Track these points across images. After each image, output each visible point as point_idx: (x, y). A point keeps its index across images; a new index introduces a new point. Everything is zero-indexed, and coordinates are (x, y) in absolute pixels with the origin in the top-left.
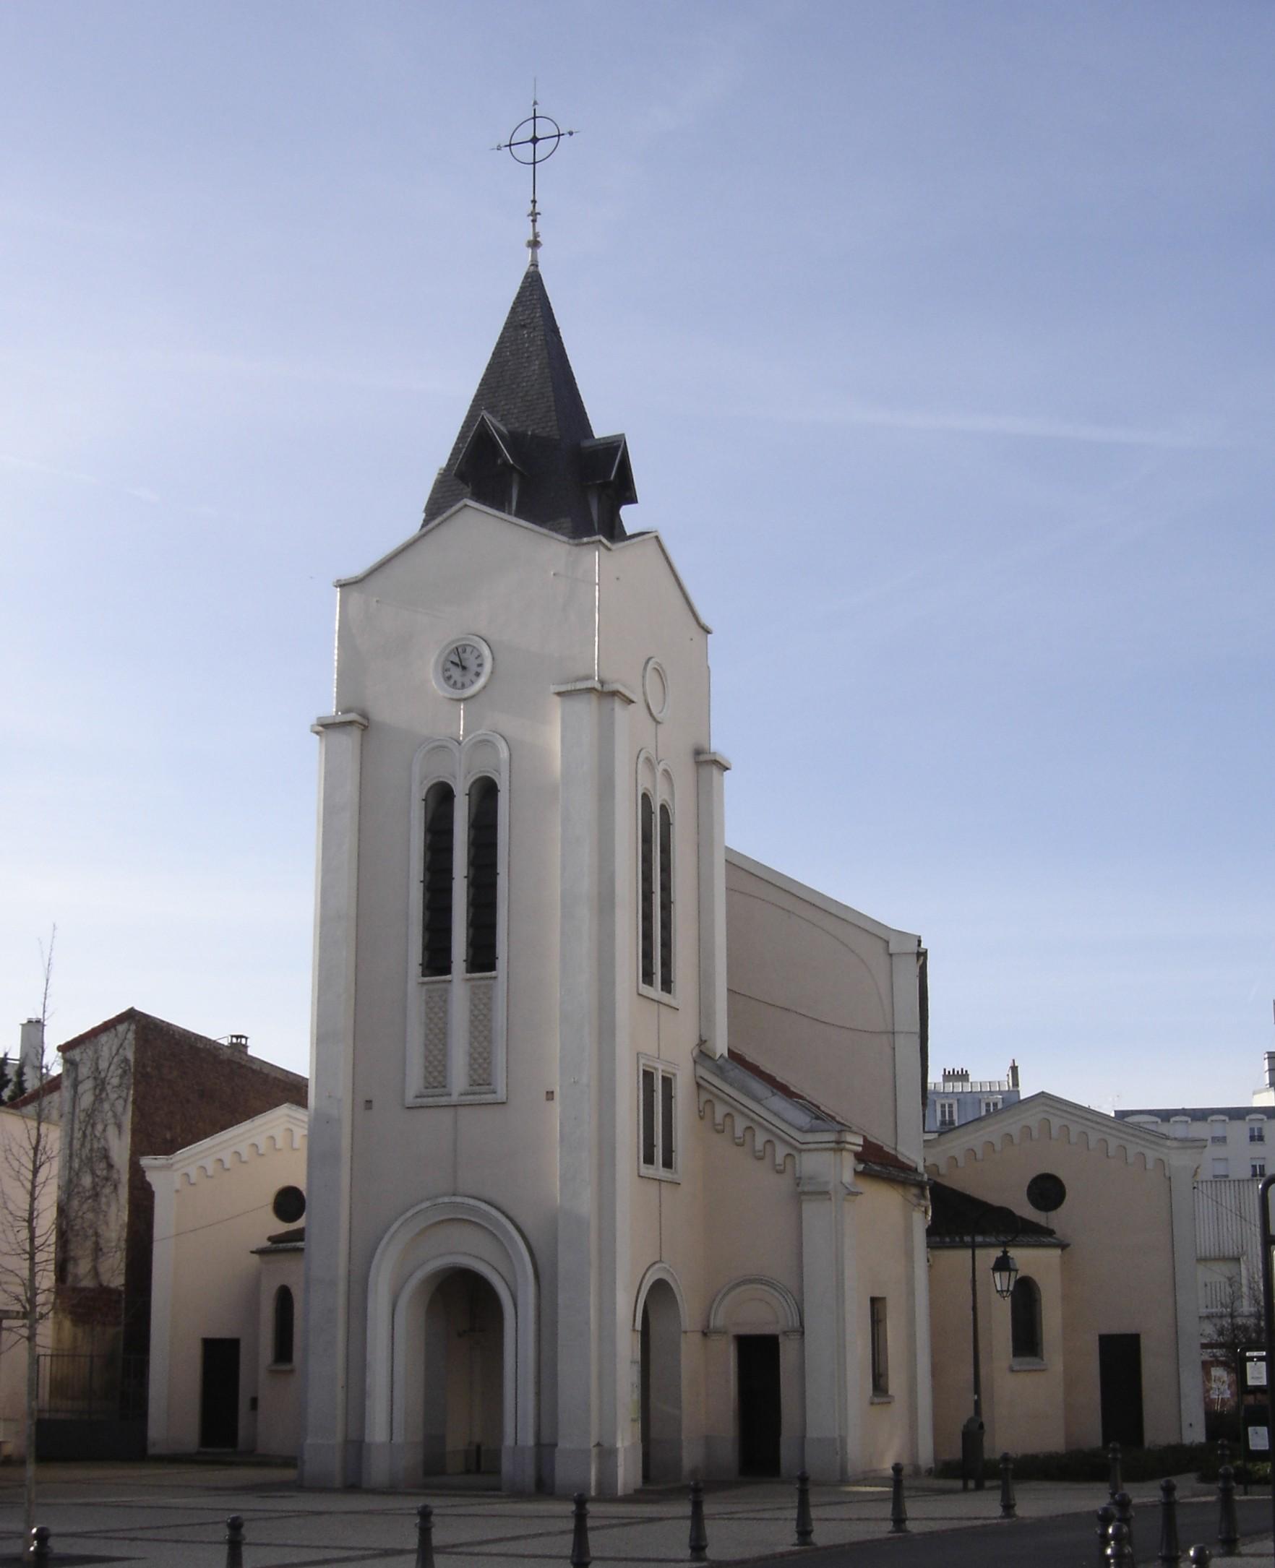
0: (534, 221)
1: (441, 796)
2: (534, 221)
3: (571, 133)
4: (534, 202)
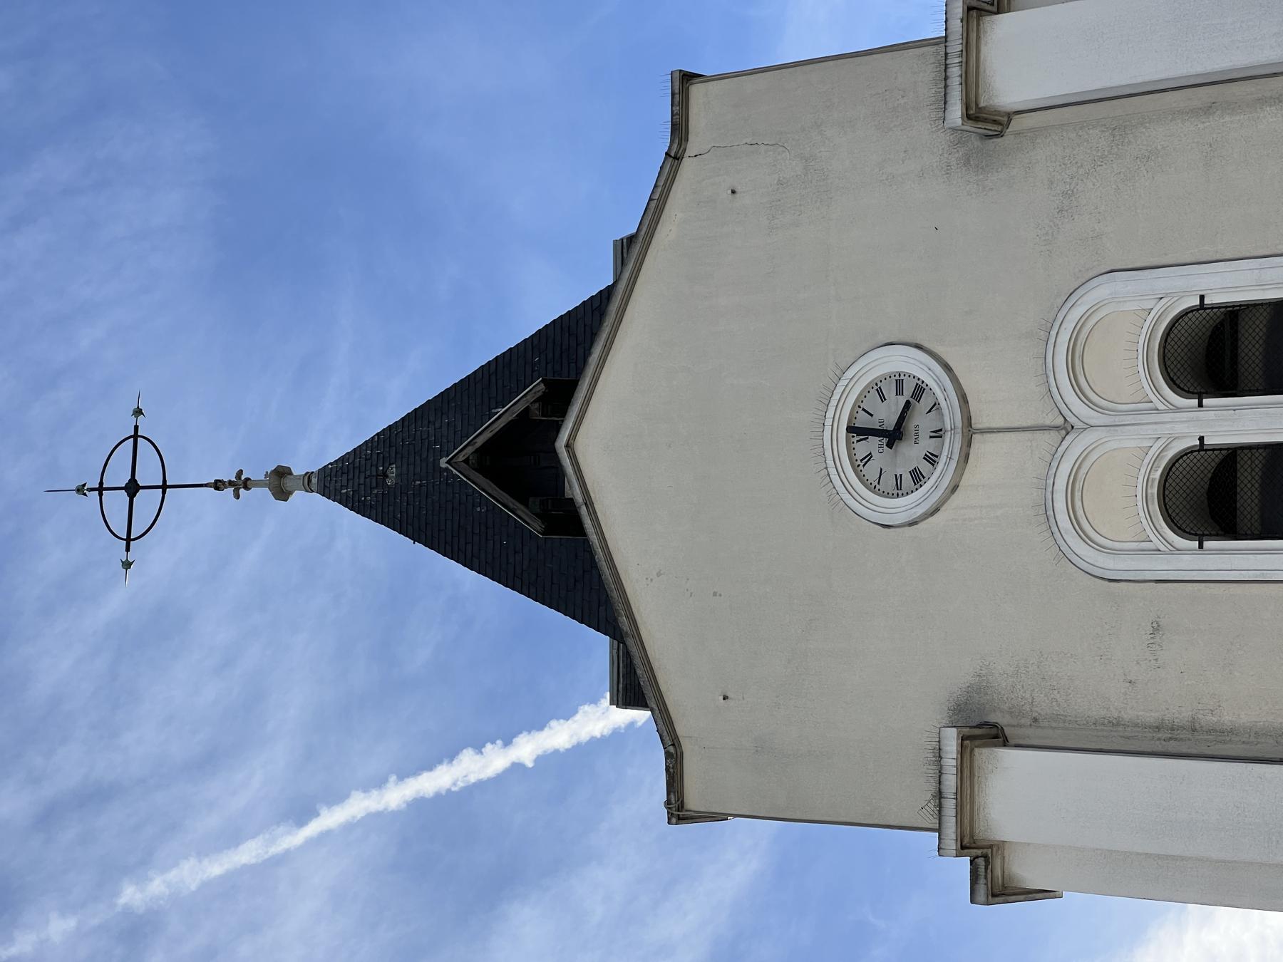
0: (247, 484)
3: (138, 412)
4: (218, 485)
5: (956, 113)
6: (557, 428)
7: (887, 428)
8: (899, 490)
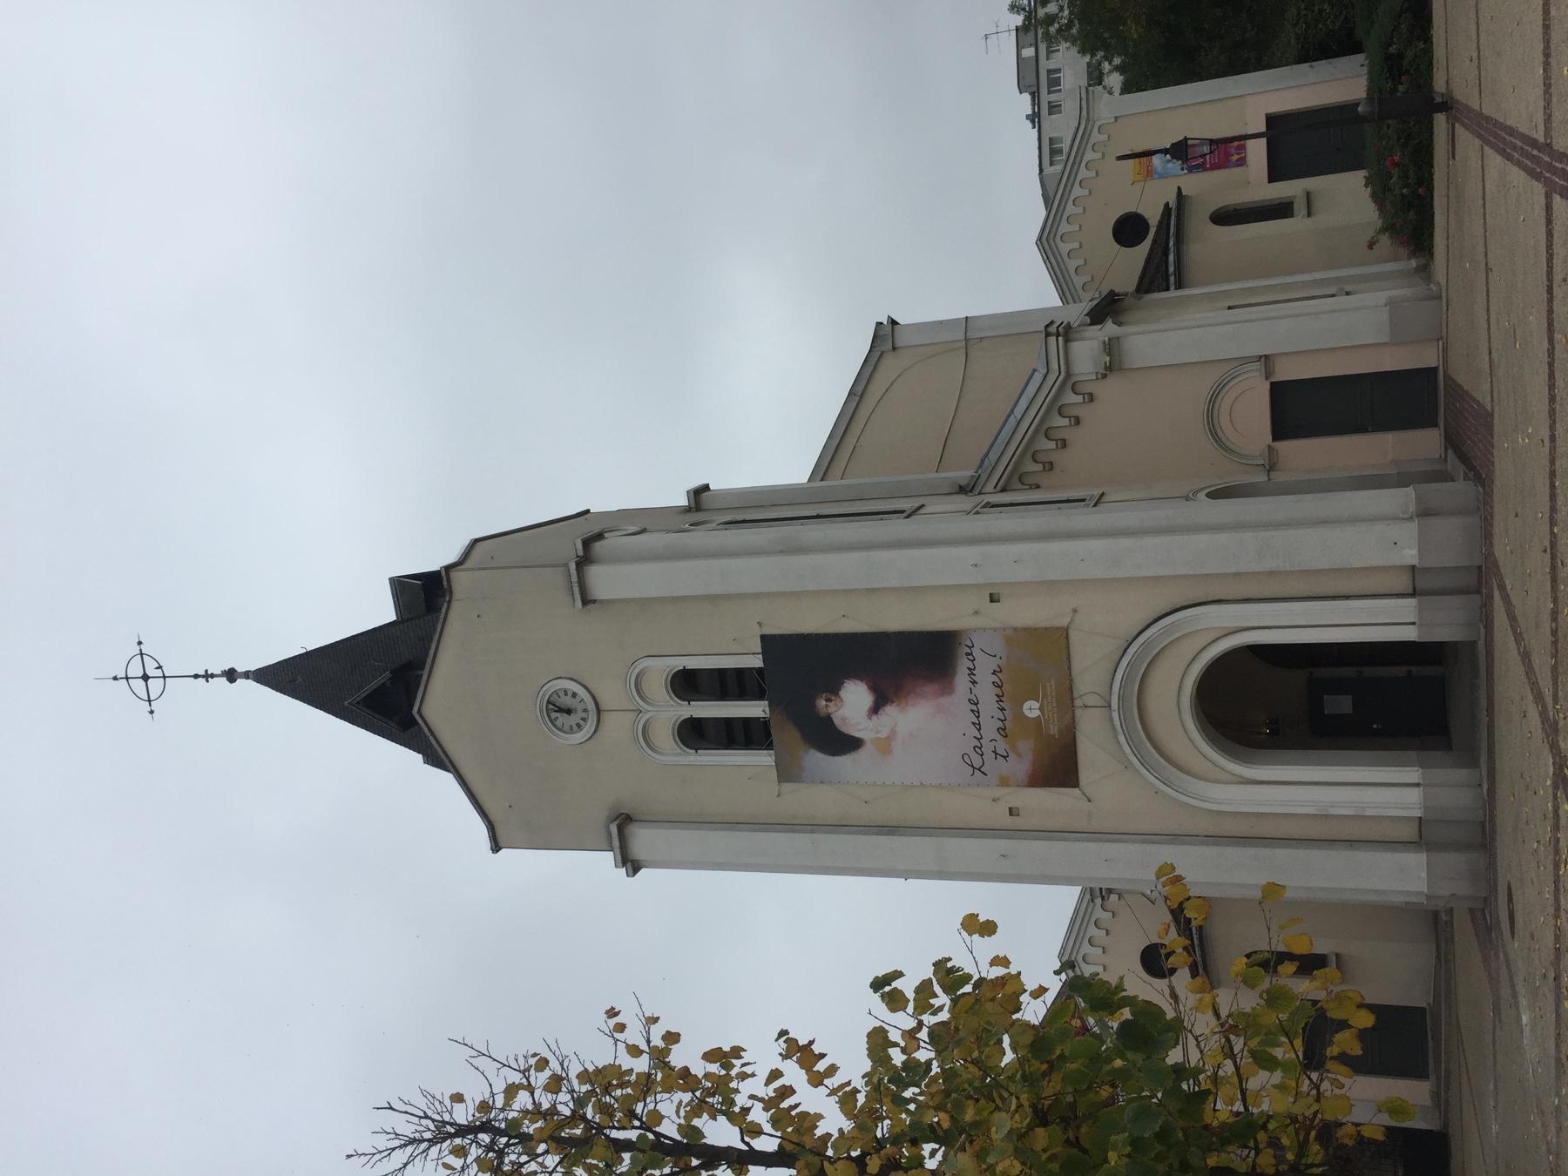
0: (212, 676)
1: (694, 734)
2: (212, 676)
3: (140, 643)
4: (196, 676)
5: (579, 603)
6: (411, 706)
7: (557, 708)
8: (571, 731)
